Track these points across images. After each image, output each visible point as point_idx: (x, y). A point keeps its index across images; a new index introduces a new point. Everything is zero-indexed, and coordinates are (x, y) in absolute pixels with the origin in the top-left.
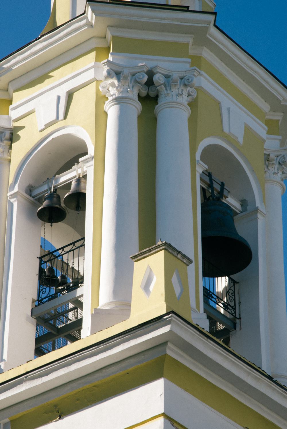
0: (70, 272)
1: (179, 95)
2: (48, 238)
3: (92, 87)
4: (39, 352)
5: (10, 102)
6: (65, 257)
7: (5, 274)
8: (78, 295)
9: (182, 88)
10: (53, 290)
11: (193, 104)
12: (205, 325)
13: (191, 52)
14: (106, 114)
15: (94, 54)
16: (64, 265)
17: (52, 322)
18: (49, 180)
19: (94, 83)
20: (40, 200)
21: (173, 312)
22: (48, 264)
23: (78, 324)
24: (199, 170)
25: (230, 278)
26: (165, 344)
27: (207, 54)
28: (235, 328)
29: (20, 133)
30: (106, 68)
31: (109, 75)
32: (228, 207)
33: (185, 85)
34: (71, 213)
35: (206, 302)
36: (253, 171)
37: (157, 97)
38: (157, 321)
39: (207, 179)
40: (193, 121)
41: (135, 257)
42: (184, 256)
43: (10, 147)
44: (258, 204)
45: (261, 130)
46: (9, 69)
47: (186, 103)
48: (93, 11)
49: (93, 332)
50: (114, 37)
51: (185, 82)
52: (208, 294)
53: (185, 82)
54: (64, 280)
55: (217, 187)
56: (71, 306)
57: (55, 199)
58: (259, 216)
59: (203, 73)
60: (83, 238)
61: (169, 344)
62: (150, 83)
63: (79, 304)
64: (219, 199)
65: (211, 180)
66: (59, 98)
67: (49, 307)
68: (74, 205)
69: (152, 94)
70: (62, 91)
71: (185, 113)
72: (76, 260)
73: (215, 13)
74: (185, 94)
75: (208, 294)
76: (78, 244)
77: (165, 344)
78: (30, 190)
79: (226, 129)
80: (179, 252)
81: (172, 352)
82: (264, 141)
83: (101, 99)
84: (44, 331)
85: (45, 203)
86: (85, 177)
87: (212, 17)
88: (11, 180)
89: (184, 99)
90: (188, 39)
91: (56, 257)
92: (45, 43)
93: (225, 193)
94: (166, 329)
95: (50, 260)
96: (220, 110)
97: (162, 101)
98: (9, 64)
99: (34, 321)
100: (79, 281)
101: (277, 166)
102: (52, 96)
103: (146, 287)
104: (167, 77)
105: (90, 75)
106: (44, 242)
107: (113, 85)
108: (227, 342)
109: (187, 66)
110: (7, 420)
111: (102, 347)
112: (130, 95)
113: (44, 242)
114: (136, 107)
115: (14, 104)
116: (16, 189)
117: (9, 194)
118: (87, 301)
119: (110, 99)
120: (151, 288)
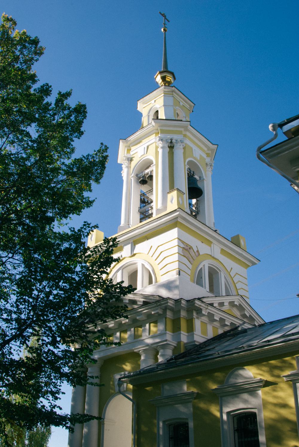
0: (149, 199)
1: (180, 146)
2: (142, 190)
3: (154, 144)
4: (141, 222)
5: (131, 150)
6: (148, 195)
7: (130, 192)
8: (152, 205)
9: (181, 143)
10: (144, 205)
11: (184, 148)
12: (189, 212)
13: (183, 133)
14: (158, 152)
15: (155, 134)
16: (148, 197)
17: (145, 214)
18: (142, 172)
19: (155, 143)
20: (140, 178)
21: (180, 208)
22: (143, 197)
23: (152, 214)
24: (187, 167)
25: (197, 200)
26: (177, 217)
27: (188, 134)
28: (198, 214)
29: (133, 159)
30: (158, 138)
31: (159, 140)
32: (195, 178)
33: (182, 143)
34: (149, 181)
35: (189, 207)
36: (202, 168)
37: (174, 146)
38: (175, 211)
39: (189, 171)
40: (184, 153)
41: (168, 193)
42: (182, 192)
43: (131, 163)
44: (204, 177)
45: (204, 156)
46: (130, 140)
47: (182, 148)
48: (154, 122)
49: (156, 215)
50: (160, 129)
51: (182, 142)
52: (190, 204)
53: (182, 142)
54: (148, 202)
55: (192, 173)
56: (150, 209)
57: (144, 178)
58: (205, 181)
59: (187, 139)
60: (153, 189)
61: (179, 218)
62: (171, 142)
63: (152, 208)
64: (192, 176)
65: (190, 171)
66: (145, 148)
67: (143, 209)
68: (150, 179)
69: (172, 146)
70: (146, 146)
71: (182, 151)
72: (151, 196)
73: (190, 122)
74: (182, 145)
75: (190, 204)
76: (151, 191)
77: (177, 217)
78: (137, 175)
79: (194, 156)
80: (181, 191)
81: (180, 220)
82: (205, 159)
83: (157, 147)
84: (142, 216)
85: (141, 179)
86: (153, 171)
87: (189, 123)
88: (131, 172)
89: (182, 147)
90: (182, 129)
91: (145, 195)
92: (140, 132)
93: (194, 174)
94: (178, 213)
95: (143, 196)
96: (192, 150)
97: (175, 148)
98: (130, 139)
99: (139, 213)
100: (152, 202)
101: (209, 166)
102: (142, 148)
103: (171, 202)
104: (176, 140)
105: (154, 141)
106: (141, 191)
107: (160, 143)
108: (196, 217)
109: (182, 137)
110: (132, 241)
111: (159, 219)
112: (165, 146)
113: (141, 191)
114: (168, 150)
115: (132, 150)
116: (133, 175)
117: (131, 176)
118: (154, 207)
119: (160, 147)
120: (173, 202)
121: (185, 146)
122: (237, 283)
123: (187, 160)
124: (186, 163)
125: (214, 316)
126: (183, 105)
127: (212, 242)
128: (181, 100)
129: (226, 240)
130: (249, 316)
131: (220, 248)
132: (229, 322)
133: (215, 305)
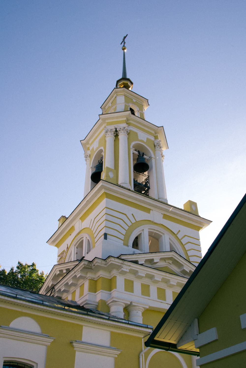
62: (116, 131)
121: (129, 132)
122: (186, 244)
123: (133, 143)
124: (131, 146)
125: (170, 281)
126: (136, 101)
127: (150, 209)
128: (133, 97)
129: (157, 202)
130: (189, 271)
131: (162, 214)
132: (144, 274)
133: (140, 263)
